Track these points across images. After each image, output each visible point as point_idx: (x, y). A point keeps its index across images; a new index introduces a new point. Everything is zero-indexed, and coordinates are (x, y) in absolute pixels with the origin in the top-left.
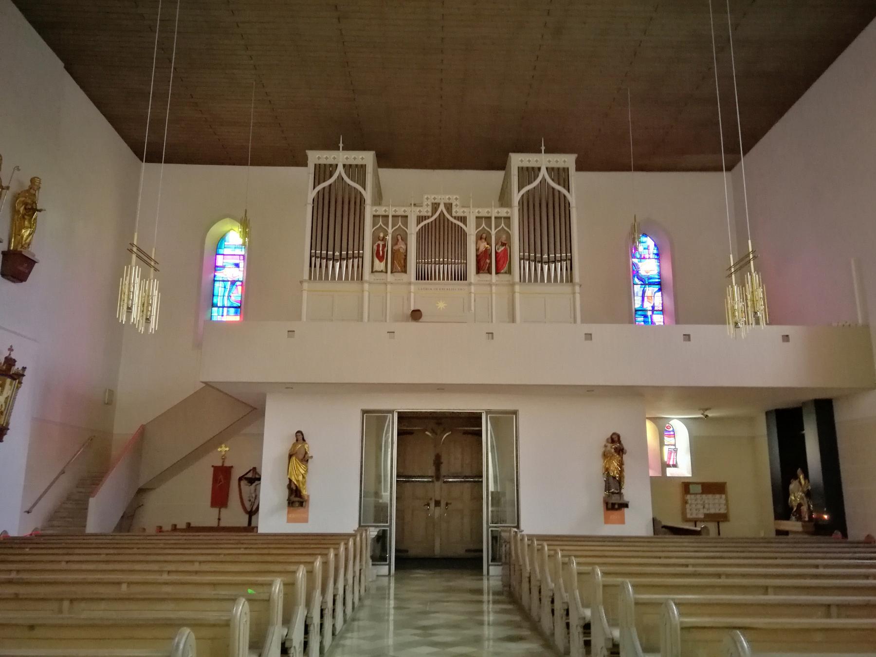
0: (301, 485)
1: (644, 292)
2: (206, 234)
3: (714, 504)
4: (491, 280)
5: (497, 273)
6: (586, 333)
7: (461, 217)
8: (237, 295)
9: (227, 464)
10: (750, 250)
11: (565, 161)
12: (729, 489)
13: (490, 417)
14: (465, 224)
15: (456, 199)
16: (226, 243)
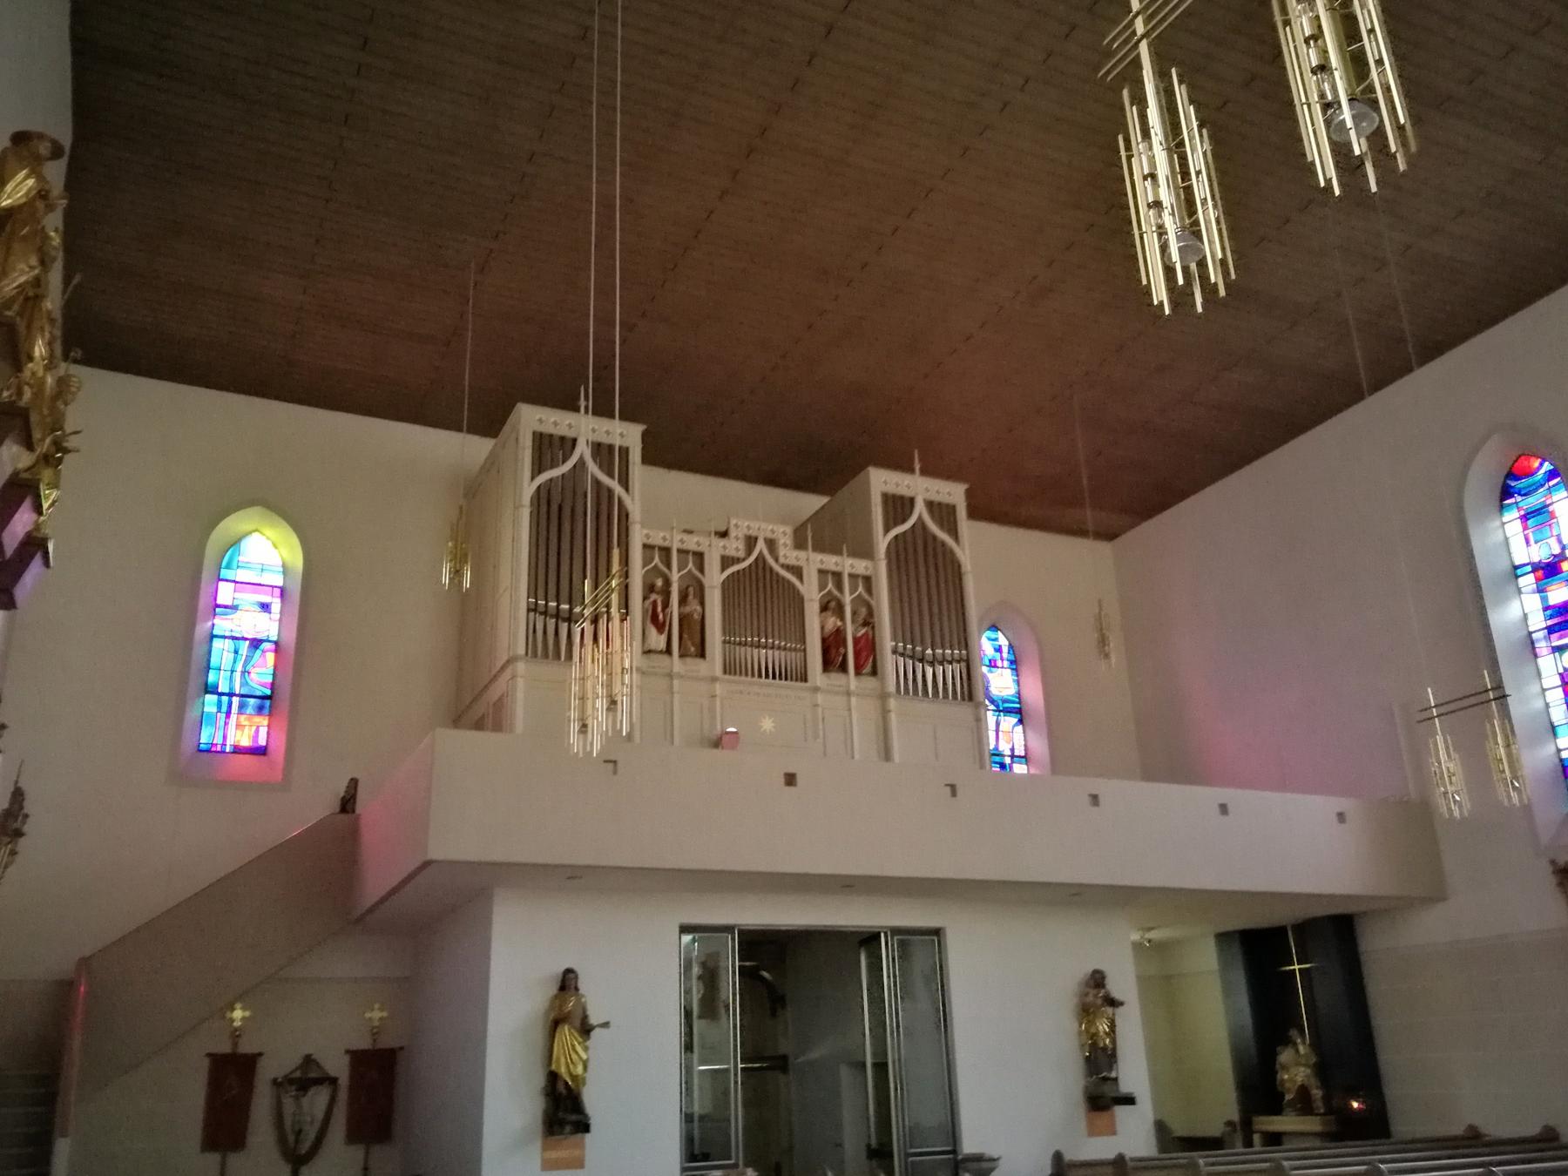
1: (998, 724)
2: (208, 535)
5: (858, 672)
6: (360, 784)
8: (263, 670)
9: (246, 1047)
13: (897, 939)
14: (800, 577)
15: (784, 533)
16: (240, 558)
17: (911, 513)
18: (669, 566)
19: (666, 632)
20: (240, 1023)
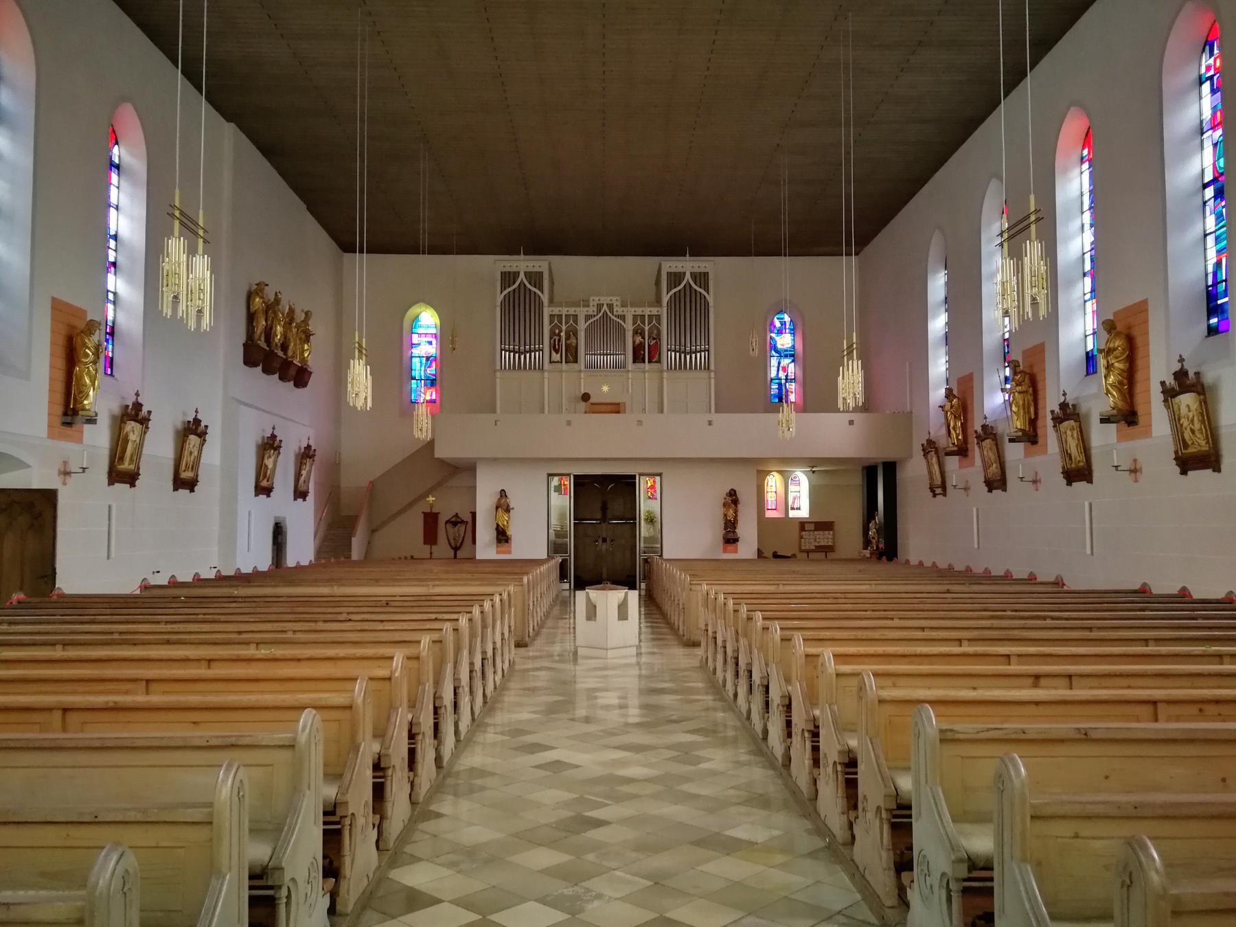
1: (779, 363)
2: (405, 313)
3: (824, 539)
5: (650, 362)
9: (435, 510)
10: (855, 341)
11: (705, 267)
12: (836, 527)
15: (617, 300)
16: (419, 323)
17: (684, 279)
18: (561, 324)
19: (560, 353)
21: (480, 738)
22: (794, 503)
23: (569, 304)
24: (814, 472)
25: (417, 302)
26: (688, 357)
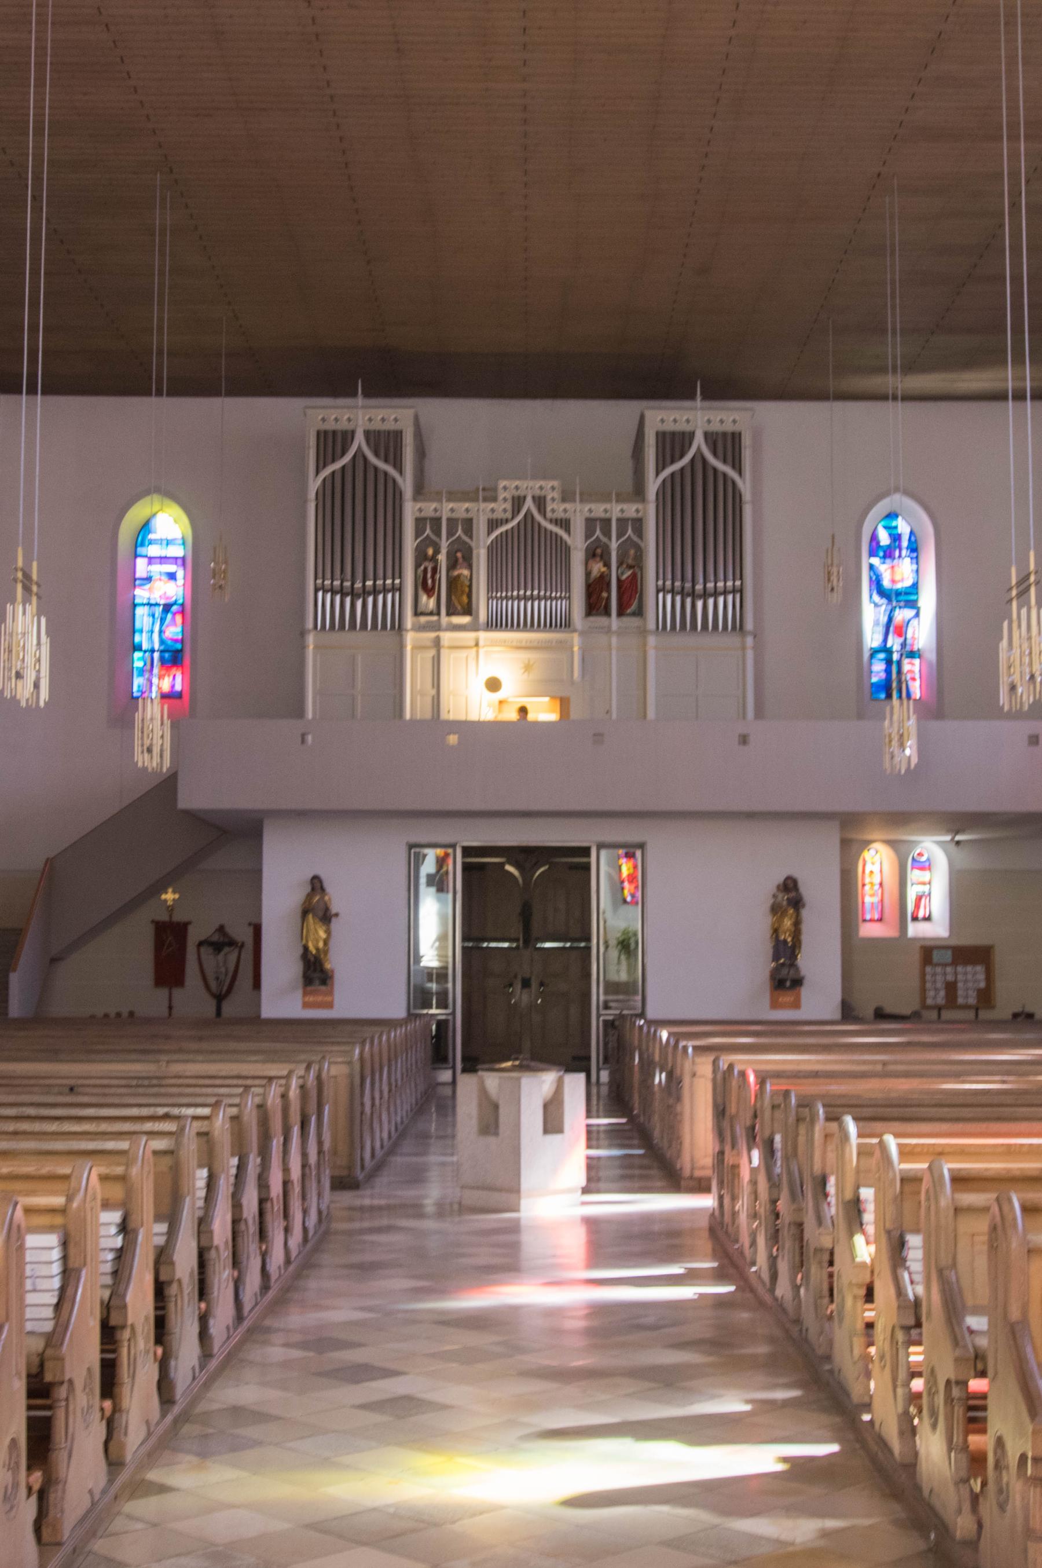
0: (322, 956)
4: (610, 627)
5: (621, 613)
7: (561, 520)
10: (1032, 567)
11: (734, 421)
14: (568, 530)
15: (553, 488)
16: (151, 536)
20: (171, 903)
21: (256, 1353)
22: (917, 906)
23: (452, 497)
24: (958, 843)
25: (147, 493)
26: (700, 604)
